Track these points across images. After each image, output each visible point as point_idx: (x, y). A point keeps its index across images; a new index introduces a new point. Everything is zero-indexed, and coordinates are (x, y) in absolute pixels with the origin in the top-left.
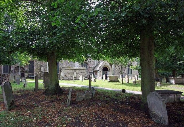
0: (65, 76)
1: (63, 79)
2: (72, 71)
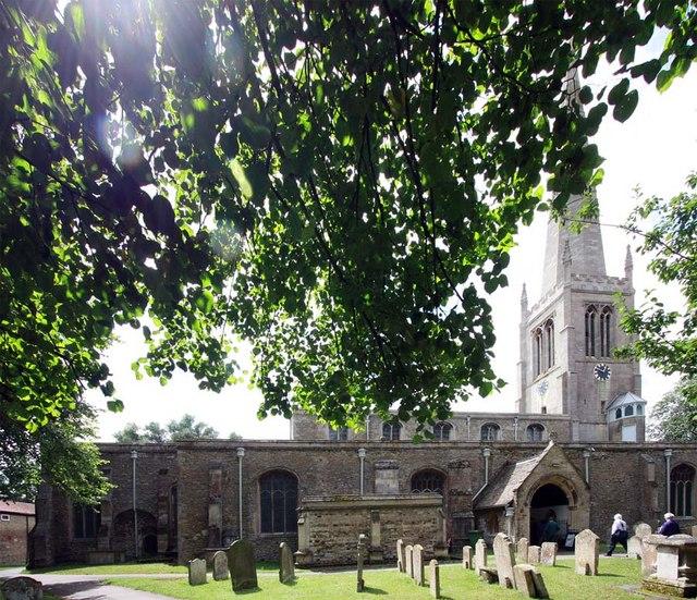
0: (323, 546)
1: (308, 560)
2: (358, 518)
